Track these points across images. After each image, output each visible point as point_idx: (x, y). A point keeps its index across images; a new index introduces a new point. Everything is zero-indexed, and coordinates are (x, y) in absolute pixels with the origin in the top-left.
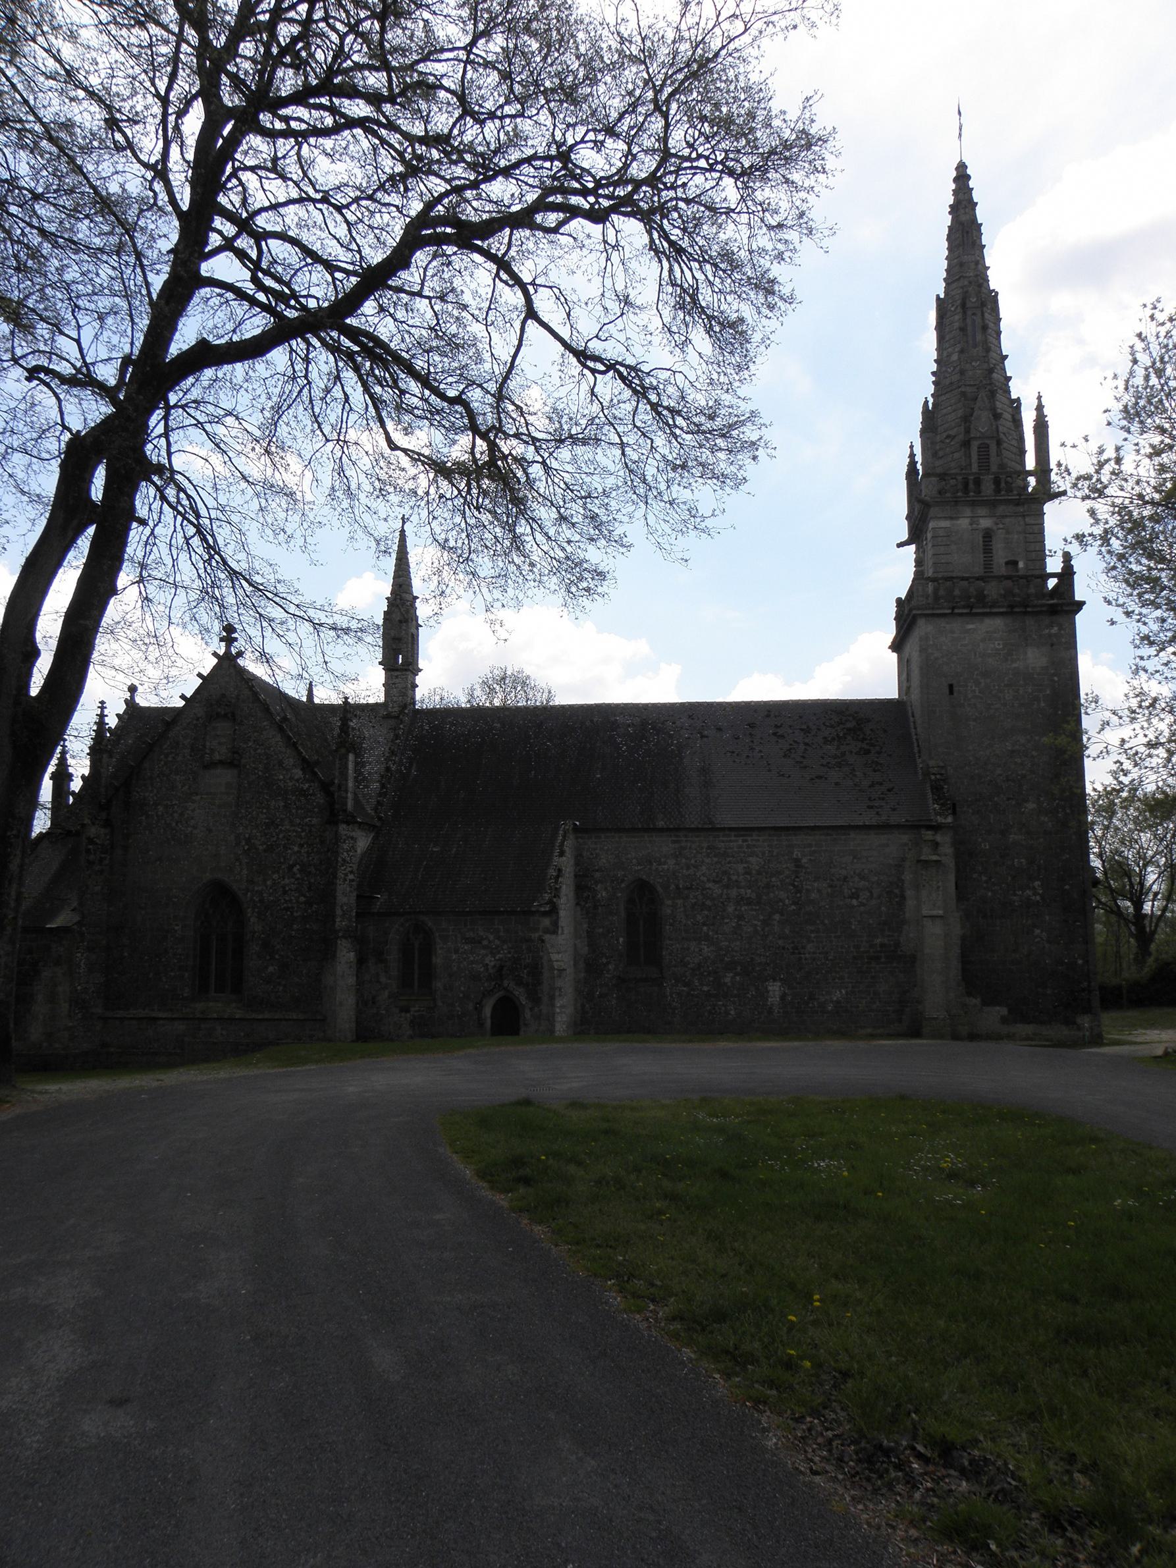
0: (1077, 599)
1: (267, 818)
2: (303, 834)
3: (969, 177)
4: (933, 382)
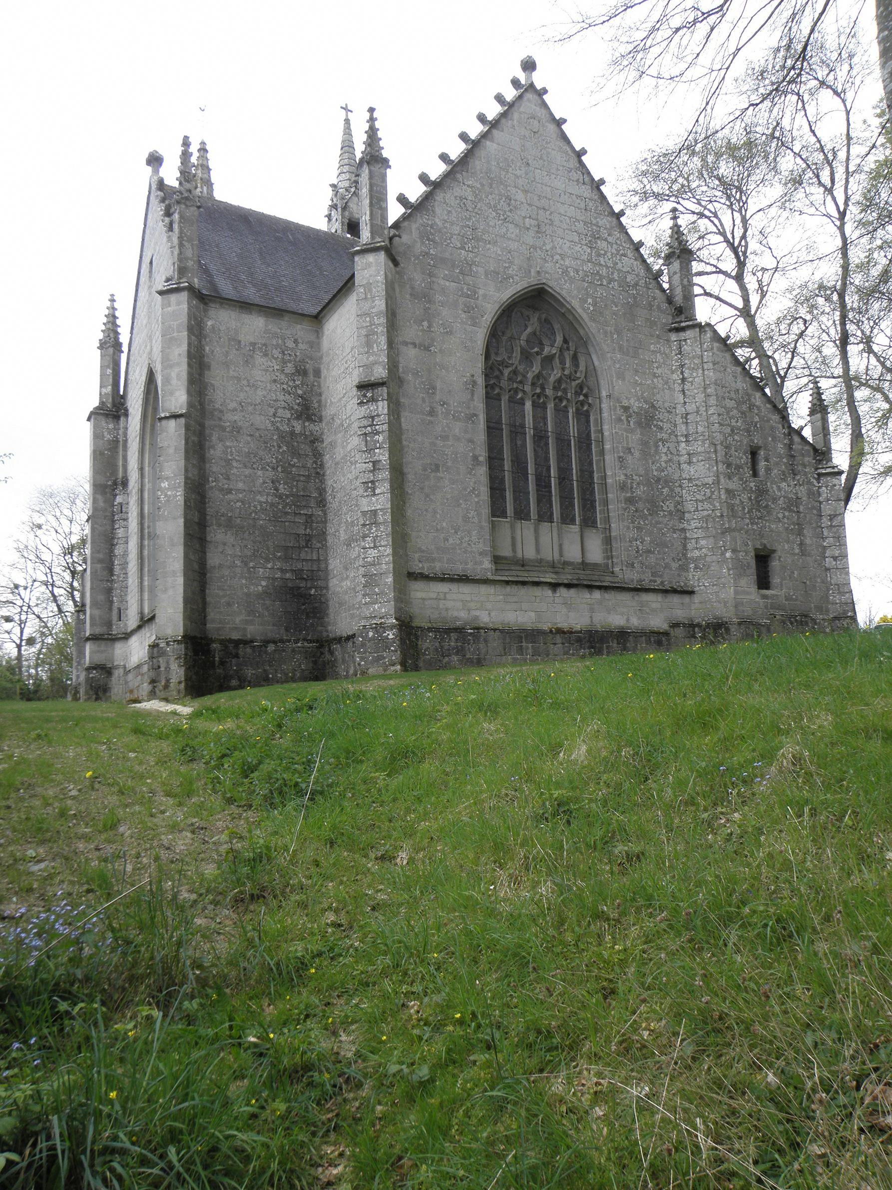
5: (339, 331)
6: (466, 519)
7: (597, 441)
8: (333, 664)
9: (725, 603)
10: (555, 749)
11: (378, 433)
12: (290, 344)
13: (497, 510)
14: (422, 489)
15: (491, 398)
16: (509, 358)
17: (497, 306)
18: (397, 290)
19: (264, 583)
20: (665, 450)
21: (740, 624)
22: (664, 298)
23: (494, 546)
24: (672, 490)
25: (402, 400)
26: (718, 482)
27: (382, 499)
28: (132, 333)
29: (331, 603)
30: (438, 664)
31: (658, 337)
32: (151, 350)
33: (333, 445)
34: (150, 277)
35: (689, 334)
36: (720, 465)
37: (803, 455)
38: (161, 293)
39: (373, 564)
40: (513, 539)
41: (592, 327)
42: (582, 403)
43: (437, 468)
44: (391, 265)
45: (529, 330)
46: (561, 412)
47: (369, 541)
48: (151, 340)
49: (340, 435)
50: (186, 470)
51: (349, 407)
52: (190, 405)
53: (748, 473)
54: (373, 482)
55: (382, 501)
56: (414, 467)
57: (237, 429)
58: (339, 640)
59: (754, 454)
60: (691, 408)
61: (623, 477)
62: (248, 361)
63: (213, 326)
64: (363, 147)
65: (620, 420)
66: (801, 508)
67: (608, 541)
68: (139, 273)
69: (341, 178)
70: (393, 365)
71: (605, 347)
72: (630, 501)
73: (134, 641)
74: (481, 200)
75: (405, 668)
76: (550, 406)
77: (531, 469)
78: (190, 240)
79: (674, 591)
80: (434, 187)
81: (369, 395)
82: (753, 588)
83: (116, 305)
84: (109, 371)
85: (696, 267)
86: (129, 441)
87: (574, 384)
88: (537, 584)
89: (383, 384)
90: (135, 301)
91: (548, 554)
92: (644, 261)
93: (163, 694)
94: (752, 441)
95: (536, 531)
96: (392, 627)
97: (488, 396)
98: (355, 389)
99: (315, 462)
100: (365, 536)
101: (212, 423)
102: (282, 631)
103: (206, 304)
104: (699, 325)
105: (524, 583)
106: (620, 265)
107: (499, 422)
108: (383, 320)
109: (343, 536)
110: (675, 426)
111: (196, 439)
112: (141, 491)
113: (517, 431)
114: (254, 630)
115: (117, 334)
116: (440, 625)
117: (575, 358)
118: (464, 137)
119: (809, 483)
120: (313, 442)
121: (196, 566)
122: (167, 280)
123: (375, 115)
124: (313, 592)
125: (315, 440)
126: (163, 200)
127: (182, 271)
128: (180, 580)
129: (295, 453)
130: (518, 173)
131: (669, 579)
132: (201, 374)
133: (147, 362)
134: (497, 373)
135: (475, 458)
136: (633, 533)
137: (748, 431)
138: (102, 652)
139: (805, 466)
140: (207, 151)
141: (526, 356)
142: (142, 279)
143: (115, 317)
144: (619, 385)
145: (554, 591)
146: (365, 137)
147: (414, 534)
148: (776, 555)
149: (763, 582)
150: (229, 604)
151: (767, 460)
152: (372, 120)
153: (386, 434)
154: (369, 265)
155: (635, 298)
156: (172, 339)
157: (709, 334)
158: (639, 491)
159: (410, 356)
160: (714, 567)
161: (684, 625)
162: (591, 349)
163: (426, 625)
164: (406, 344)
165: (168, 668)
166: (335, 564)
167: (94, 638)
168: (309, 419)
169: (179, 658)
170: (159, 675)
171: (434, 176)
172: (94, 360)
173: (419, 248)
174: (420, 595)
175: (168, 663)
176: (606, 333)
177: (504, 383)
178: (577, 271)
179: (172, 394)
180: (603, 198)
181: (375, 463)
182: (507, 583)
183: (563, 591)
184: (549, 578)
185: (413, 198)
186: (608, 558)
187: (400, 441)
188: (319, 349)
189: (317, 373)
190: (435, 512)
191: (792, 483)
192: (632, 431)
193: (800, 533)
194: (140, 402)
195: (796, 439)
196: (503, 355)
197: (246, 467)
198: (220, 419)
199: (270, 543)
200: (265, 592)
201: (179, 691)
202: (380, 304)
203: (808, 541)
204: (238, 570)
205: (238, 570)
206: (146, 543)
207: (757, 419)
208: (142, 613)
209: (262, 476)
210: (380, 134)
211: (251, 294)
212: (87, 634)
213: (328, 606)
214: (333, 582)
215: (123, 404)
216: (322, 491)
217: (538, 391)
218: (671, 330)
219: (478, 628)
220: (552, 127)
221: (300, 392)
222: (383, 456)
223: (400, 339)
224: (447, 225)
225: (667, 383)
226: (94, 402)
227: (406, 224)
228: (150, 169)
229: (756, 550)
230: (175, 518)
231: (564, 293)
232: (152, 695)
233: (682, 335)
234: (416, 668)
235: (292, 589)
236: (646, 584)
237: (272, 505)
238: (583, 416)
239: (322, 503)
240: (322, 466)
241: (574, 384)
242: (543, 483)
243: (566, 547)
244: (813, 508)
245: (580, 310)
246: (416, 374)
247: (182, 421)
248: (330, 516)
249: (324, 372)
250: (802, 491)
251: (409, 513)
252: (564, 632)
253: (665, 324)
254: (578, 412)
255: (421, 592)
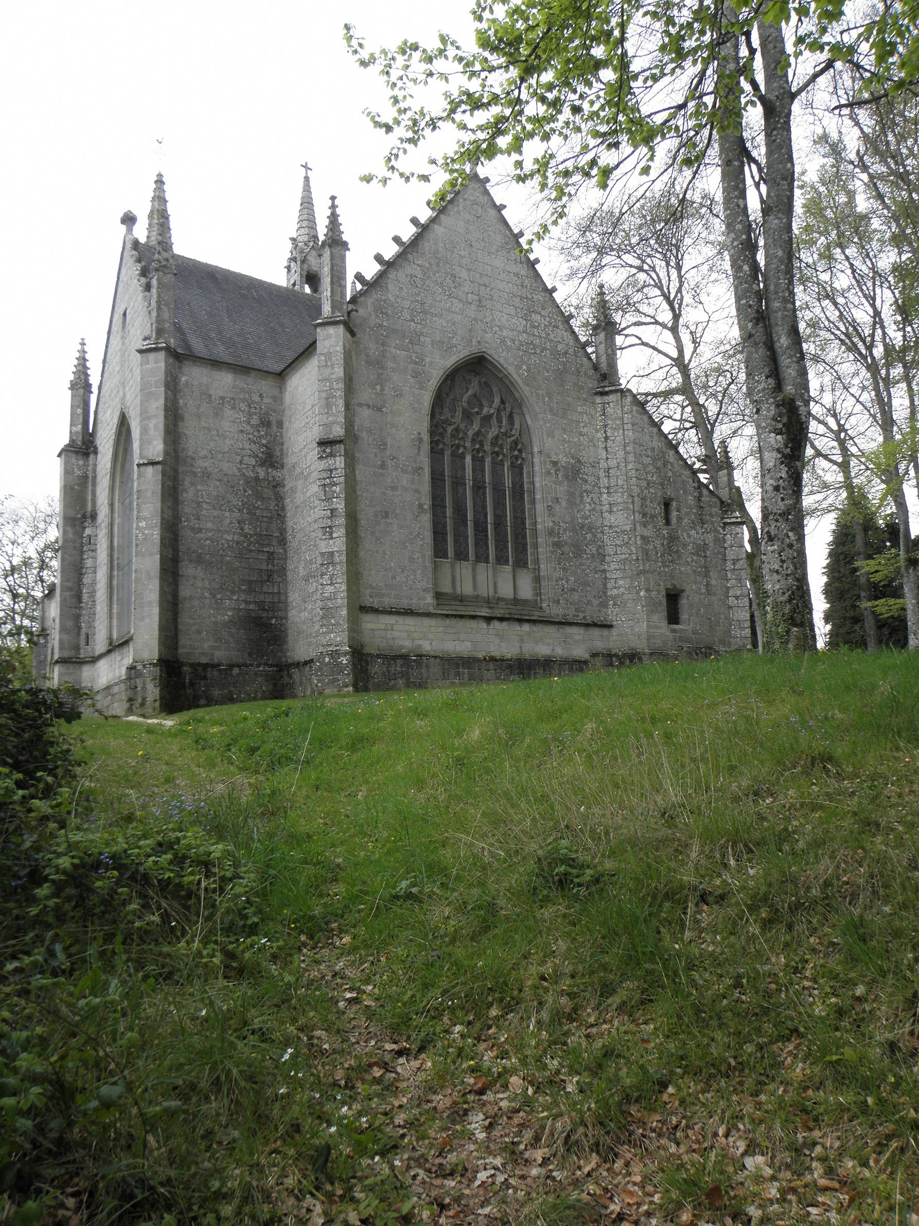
5: (300, 389)
6: (412, 560)
7: (529, 492)
8: (291, 686)
9: (639, 636)
10: (460, 733)
11: (335, 484)
12: (256, 398)
13: (439, 551)
14: (373, 533)
15: (435, 452)
16: (453, 417)
17: (441, 372)
18: (354, 358)
19: (230, 613)
20: (589, 500)
21: (651, 654)
22: (590, 366)
23: (436, 584)
24: (595, 536)
25: (357, 455)
26: (635, 529)
27: (338, 541)
28: (102, 376)
29: (290, 632)
30: (386, 686)
31: (585, 400)
32: (124, 396)
33: (293, 490)
34: (123, 328)
35: (612, 397)
36: (637, 515)
37: (711, 506)
38: (140, 351)
39: (330, 599)
40: (453, 577)
41: (525, 390)
42: (517, 458)
43: (386, 515)
44: (349, 336)
45: (470, 392)
46: (497, 465)
47: (326, 580)
48: (124, 387)
49: (300, 482)
50: (162, 512)
51: (309, 458)
52: (166, 453)
53: (661, 522)
54: (330, 527)
55: (338, 544)
56: (366, 514)
57: (207, 475)
58: (297, 665)
59: (667, 505)
60: (612, 463)
61: (551, 524)
62: (217, 414)
63: (187, 381)
64: (325, 231)
65: (549, 473)
66: (708, 553)
67: (537, 580)
68: (111, 321)
69: (300, 232)
70: (349, 425)
71: (537, 408)
72: (557, 545)
73: (102, 664)
74: (429, 277)
75: (357, 689)
76: (488, 460)
77: (470, 516)
78: (167, 304)
79: (595, 625)
80: (388, 266)
81: (328, 450)
82: (664, 623)
83: (86, 348)
84: (79, 411)
85: (619, 340)
86: (99, 478)
87: (509, 440)
88: (473, 617)
89: (340, 442)
90: (107, 347)
91: (484, 591)
92: (573, 332)
93: (139, 711)
95: (474, 570)
96: (345, 654)
97: (432, 451)
98: (315, 445)
99: (277, 505)
100: (322, 575)
101: (185, 468)
102: (246, 656)
103: (180, 361)
104: (622, 391)
105: (462, 617)
106: (552, 336)
107: (443, 474)
108: (341, 385)
109: (302, 572)
110: (599, 479)
111: (170, 483)
112: (111, 525)
113: (458, 482)
114: (221, 655)
115: (87, 375)
116: (387, 652)
117: (511, 417)
118: (414, 221)
119: (716, 530)
120: (275, 487)
121: (170, 598)
122: (145, 339)
123: (336, 202)
124: (273, 621)
125: (277, 485)
126: (139, 261)
127: (160, 332)
128: (156, 610)
129: (259, 496)
130: (463, 253)
131: (590, 614)
132: (176, 425)
133: (119, 407)
134: (441, 430)
135: (421, 506)
136: (561, 574)
137: (662, 484)
138: (71, 674)
139: (712, 516)
140: (164, 183)
141: (468, 416)
142: (114, 328)
143: (85, 360)
144: (549, 442)
145: (489, 624)
146: (327, 222)
147: (365, 573)
148: (684, 595)
149: (673, 618)
150: (198, 632)
151: (678, 511)
152: (333, 207)
153: (343, 485)
154: (329, 336)
155: (565, 365)
156: (150, 393)
157: (629, 399)
158: (566, 537)
159: (364, 416)
160: (630, 604)
161: (603, 655)
162: (525, 410)
163: (375, 652)
164: (360, 405)
165: (144, 688)
166: (294, 597)
167: (62, 661)
168: (272, 466)
169: (154, 679)
170: (136, 694)
171: (387, 256)
172: (64, 400)
173: (373, 321)
174: (370, 626)
175: (144, 683)
176: (538, 395)
177: (447, 440)
178: (514, 341)
179: (149, 443)
180: (537, 275)
181: (332, 511)
182: (447, 616)
183: (496, 624)
184: (484, 612)
185: (369, 275)
186: (537, 595)
187: (355, 491)
188: (282, 403)
189: (280, 424)
190: (385, 554)
191: (700, 531)
192: (560, 483)
193: (706, 575)
194: (111, 442)
195: (705, 492)
196: (447, 414)
197: (215, 508)
198: (192, 466)
199: (236, 578)
200: (231, 621)
201: (154, 709)
202: (339, 372)
203: (713, 582)
204: (207, 601)
205: (207, 601)
206: (115, 573)
207: (670, 474)
208: (110, 639)
209: (229, 517)
210: (340, 220)
211: (221, 352)
212: (56, 657)
213: (286, 636)
214: (292, 613)
215: (92, 442)
216: (283, 531)
217: (477, 446)
218: (596, 394)
219: (421, 656)
220: (493, 212)
221: (264, 442)
222: (340, 505)
223: (356, 401)
224: (399, 300)
225: (591, 441)
226: (64, 439)
227: (362, 299)
228: (124, 227)
229: (667, 589)
230: (151, 555)
231: (501, 361)
232: (130, 711)
233: (606, 399)
234: (366, 689)
235: (255, 618)
236: (570, 618)
237: (238, 543)
238: (518, 470)
239: (283, 542)
240: (283, 508)
241: (509, 440)
242: (480, 528)
243: (499, 585)
244: (719, 553)
245: (515, 376)
246: (369, 432)
247: (159, 467)
248: (290, 554)
249: (286, 425)
250: (709, 538)
251: (362, 554)
252: (496, 660)
253: (592, 389)
254: (513, 465)
255: (370, 623)
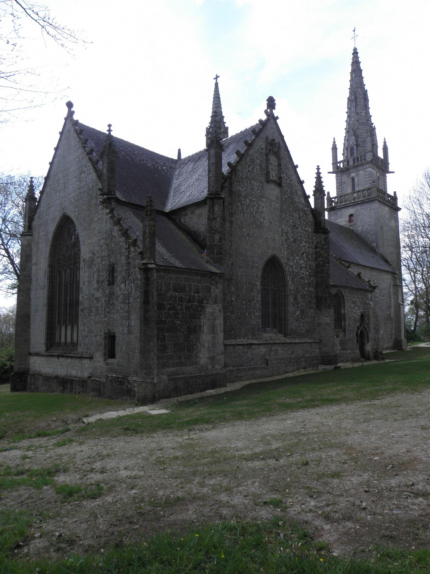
0: (335, 174)
1: (293, 223)
2: (306, 236)
3: (358, 53)
4: (275, 109)
41: (76, 222)
94: (110, 261)
234: (24, 389)
